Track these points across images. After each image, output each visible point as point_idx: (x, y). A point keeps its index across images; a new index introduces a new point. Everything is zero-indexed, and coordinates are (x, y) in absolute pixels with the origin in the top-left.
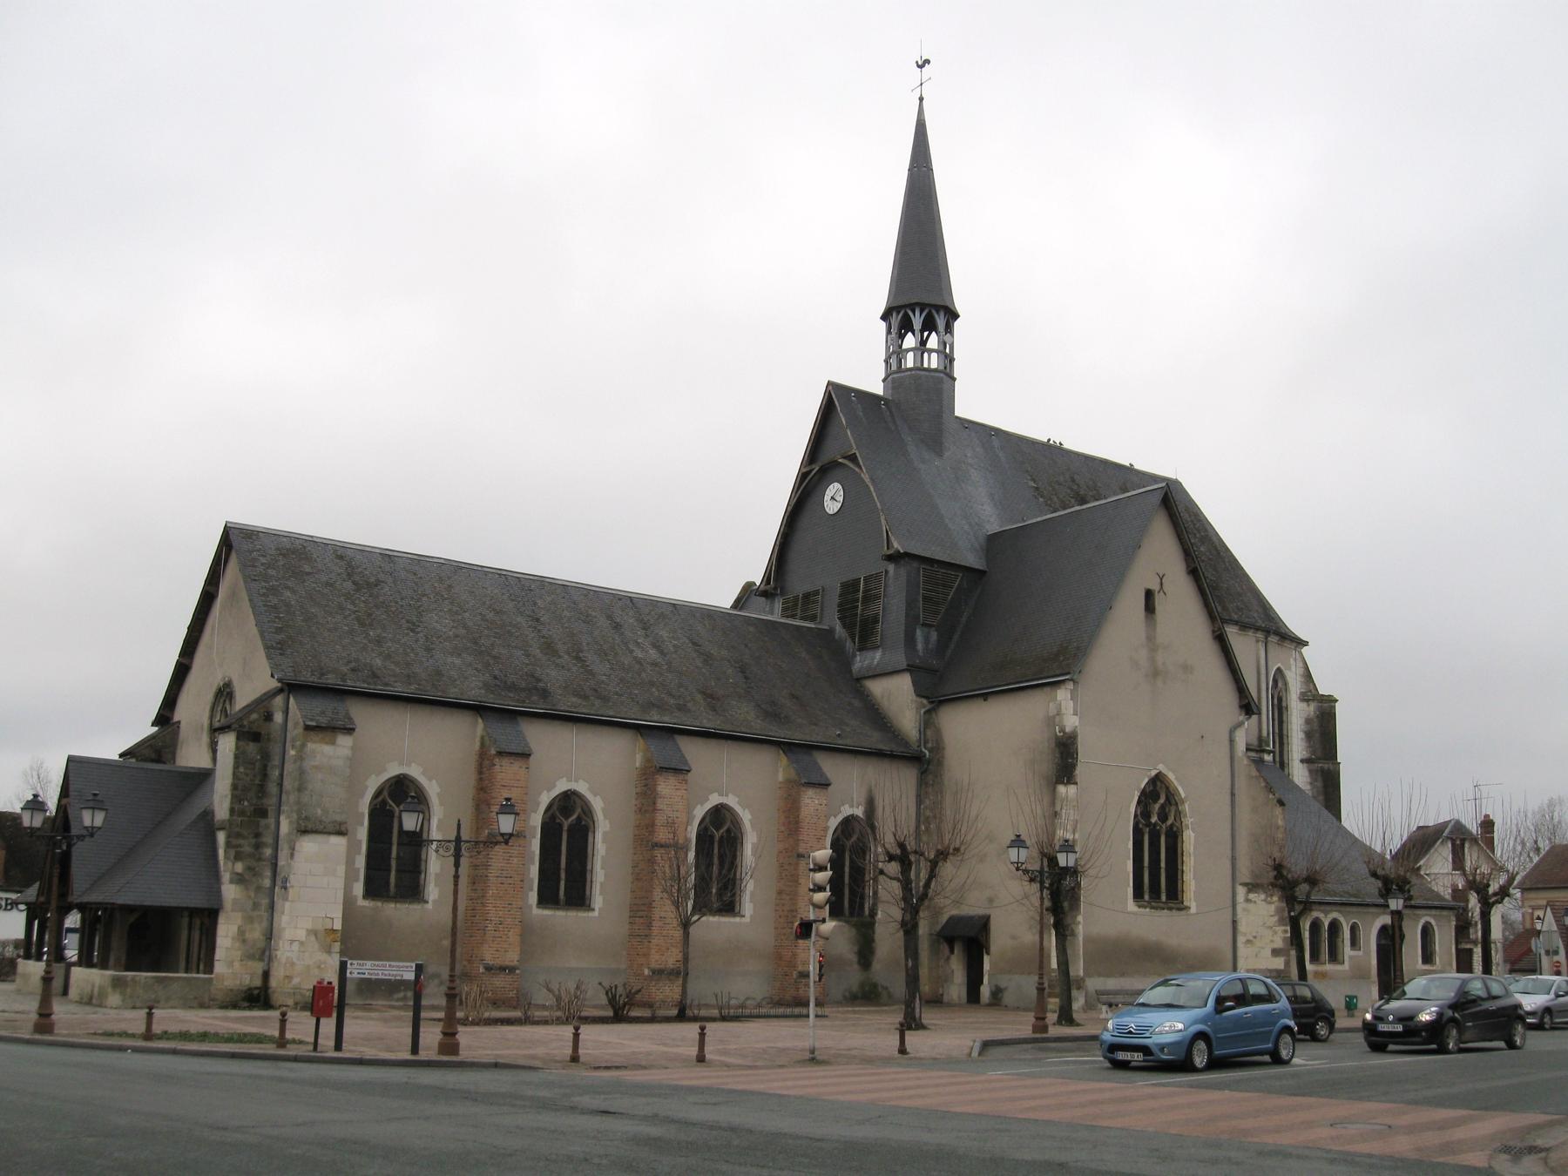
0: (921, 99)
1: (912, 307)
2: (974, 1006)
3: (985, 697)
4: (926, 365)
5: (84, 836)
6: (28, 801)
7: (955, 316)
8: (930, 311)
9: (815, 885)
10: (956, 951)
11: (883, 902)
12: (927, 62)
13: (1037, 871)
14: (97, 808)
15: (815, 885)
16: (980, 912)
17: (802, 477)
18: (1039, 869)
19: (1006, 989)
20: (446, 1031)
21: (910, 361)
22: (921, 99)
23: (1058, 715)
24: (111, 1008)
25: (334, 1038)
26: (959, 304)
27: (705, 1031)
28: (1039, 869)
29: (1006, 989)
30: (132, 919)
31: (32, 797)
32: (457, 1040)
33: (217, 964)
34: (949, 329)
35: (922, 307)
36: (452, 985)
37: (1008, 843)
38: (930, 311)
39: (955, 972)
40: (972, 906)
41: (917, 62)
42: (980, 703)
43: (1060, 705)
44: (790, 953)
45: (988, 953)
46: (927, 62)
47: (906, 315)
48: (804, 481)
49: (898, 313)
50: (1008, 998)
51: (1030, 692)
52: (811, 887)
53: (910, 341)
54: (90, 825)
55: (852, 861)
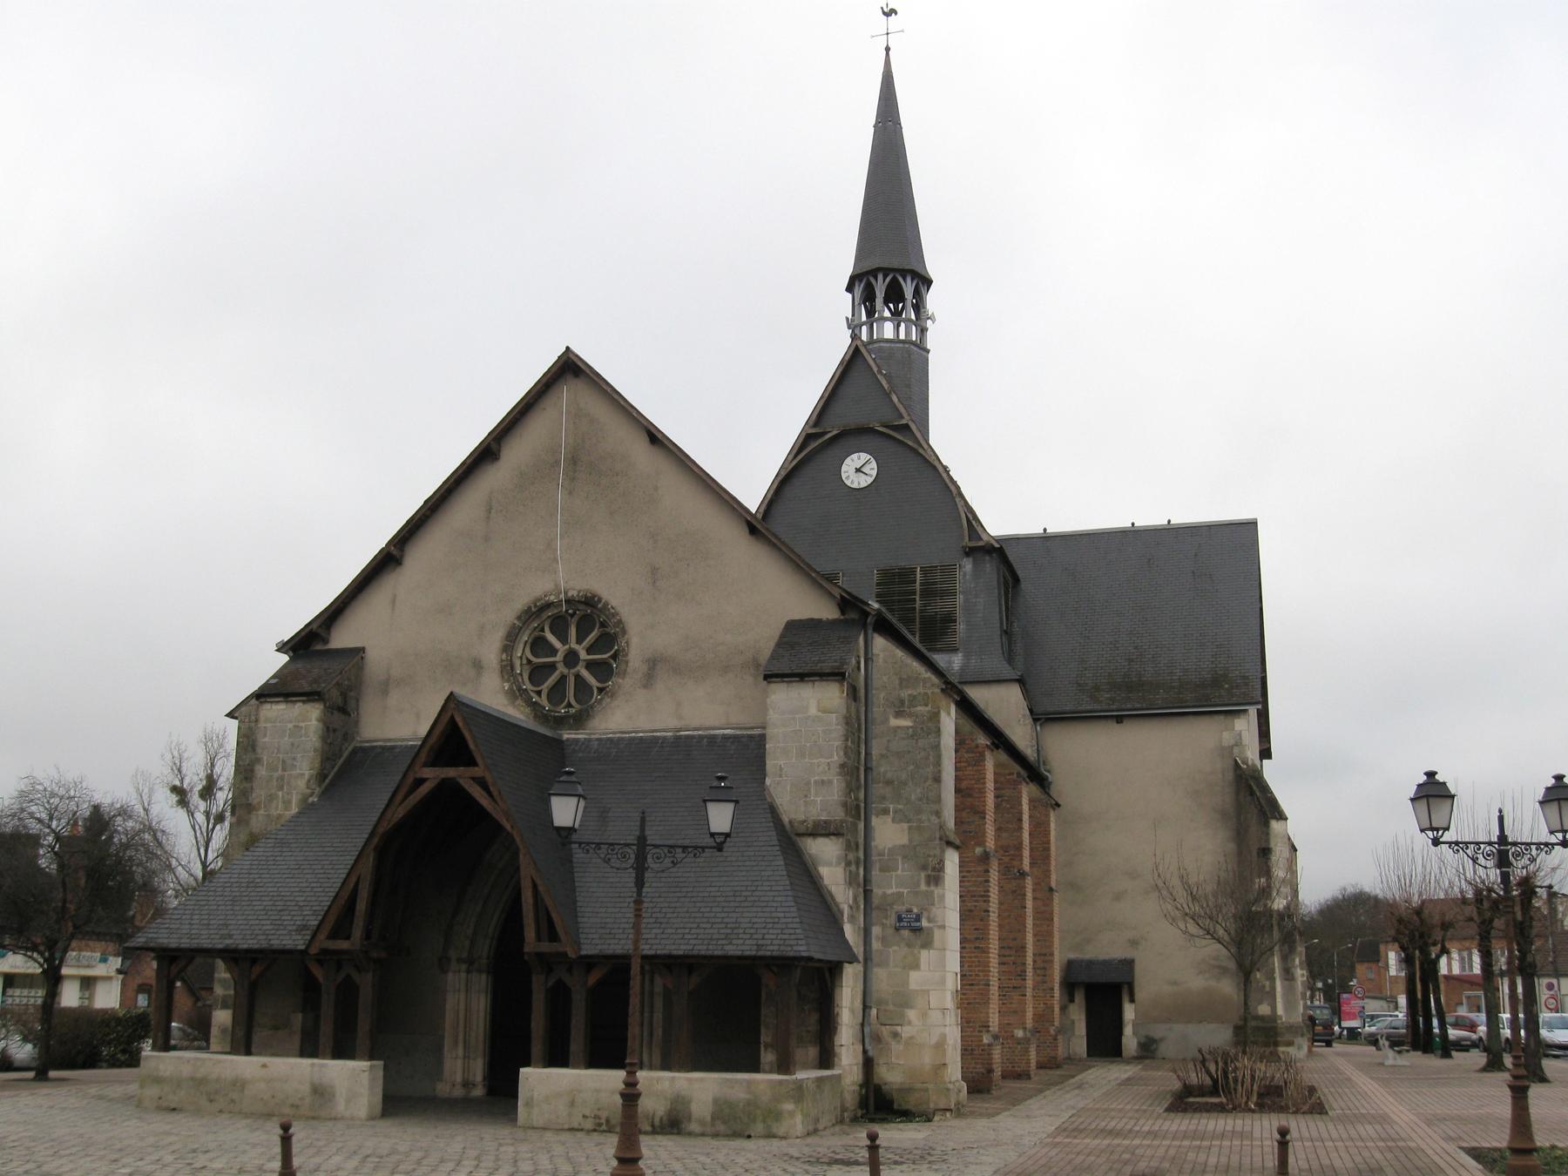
0: (888, 49)
1: (874, 273)
2: (1117, 1059)
3: (1119, 719)
5: (1553, 845)
6: (1548, 789)
8: (894, 280)
10: (1076, 1000)
11: (636, 942)
12: (893, 12)
14: (711, 801)
16: (1117, 953)
17: (806, 439)
19: (1162, 1040)
22: (888, 49)
23: (1237, 745)
24: (797, 1138)
25: (279, 1157)
29: (1162, 1040)
30: (592, 979)
31: (1553, 781)
33: (211, 1045)
35: (886, 271)
36: (631, 1080)
38: (868, 280)
39: (1077, 1024)
40: (1106, 948)
41: (882, 8)
42: (1113, 725)
43: (1240, 735)
44: (1042, 1005)
45: (1132, 1000)
46: (893, 12)
47: (895, 282)
50: (1164, 1049)
51: (1191, 718)
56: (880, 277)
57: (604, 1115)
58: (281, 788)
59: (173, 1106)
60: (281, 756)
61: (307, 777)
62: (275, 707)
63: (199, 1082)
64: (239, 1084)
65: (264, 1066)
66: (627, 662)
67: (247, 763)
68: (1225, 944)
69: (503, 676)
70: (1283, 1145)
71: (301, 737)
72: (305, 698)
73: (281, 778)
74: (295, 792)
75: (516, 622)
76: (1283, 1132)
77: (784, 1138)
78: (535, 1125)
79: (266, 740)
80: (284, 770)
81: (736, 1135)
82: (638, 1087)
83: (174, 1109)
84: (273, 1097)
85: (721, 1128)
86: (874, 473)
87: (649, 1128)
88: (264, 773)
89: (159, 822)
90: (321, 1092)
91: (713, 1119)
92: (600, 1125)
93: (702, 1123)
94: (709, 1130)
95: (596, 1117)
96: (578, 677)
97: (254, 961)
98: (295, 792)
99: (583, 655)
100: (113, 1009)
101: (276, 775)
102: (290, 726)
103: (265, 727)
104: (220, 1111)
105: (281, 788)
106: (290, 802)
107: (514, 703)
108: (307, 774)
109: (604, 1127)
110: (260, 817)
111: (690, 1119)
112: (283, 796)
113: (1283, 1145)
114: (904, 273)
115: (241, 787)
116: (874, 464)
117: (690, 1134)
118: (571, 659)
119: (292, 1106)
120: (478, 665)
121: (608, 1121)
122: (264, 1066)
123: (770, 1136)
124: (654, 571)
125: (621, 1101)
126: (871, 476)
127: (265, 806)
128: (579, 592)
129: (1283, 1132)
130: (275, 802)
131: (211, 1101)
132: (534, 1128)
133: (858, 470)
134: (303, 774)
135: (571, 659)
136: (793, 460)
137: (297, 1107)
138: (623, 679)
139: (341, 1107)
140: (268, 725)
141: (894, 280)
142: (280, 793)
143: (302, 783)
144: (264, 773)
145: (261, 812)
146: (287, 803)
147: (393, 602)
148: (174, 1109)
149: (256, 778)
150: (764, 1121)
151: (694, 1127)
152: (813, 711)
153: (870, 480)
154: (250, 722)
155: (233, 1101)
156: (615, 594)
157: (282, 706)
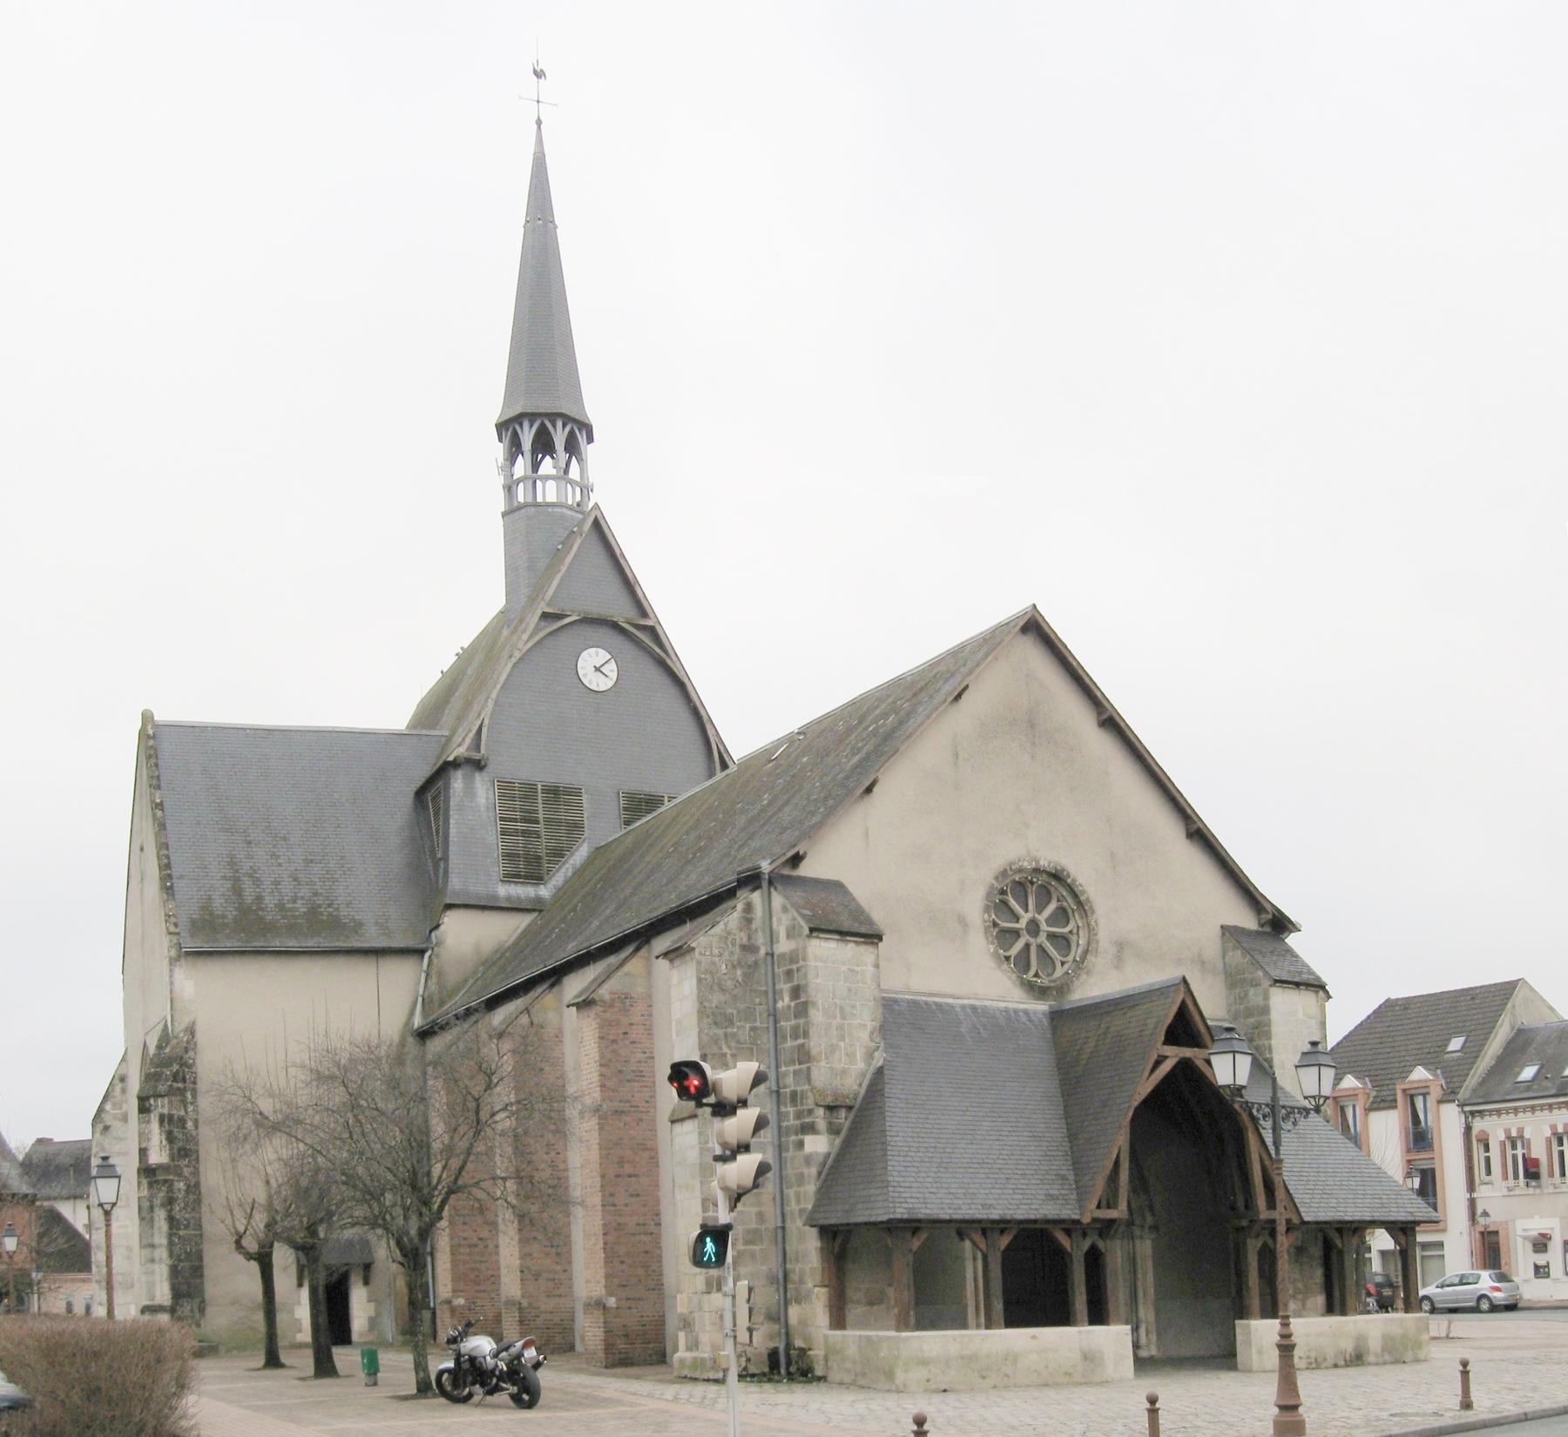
0: (539, 122)
4: (540, 499)
7: (588, 429)
8: (543, 425)
9: (724, 1145)
13: (1267, 1105)
15: (724, 1145)
18: (1268, 1100)
20: (1283, 1403)
21: (521, 495)
22: (539, 122)
26: (593, 411)
27: (1468, 1368)
28: (1268, 1100)
32: (1301, 1415)
34: (572, 447)
35: (532, 417)
36: (1285, 1332)
37: (1296, 1059)
48: (536, 634)
49: (507, 430)
52: (718, 1151)
53: (521, 467)
54: (1232, 1082)
55: (1521, 1092)
56: (559, 424)
57: (1313, 1355)
58: (842, 1038)
59: (943, 1387)
60: (838, 1002)
61: (869, 1028)
62: (824, 944)
63: (969, 1360)
64: (1011, 1358)
65: (1034, 1337)
66: (1098, 942)
67: (714, 1005)
68: (780, 1246)
69: (987, 938)
70: (1153, 1412)
71: (858, 982)
72: (862, 940)
73: (840, 1027)
74: (858, 1044)
75: (994, 882)
76: (1153, 1400)
77: (1425, 1361)
78: (1268, 1368)
79: (819, 981)
80: (843, 1017)
81: (1396, 1362)
82: (1293, 1338)
83: (945, 1391)
84: (1047, 1367)
85: (1387, 1357)
86: (614, 676)
87: (1343, 1363)
88: (820, 1019)
89: (338, 1064)
90: (1090, 1358)
91: (1383, 1351)
92: (1311, 1363)
93: (1376, 1355)
94: (1381, 1360)
95: (1308, 1357)
96: (1041, 948)
97: (915, 1231)
98: (858, 1044)
99: (1044, 927)
100: (675, 1306)
101: (834, 1023)
102: (844, 968)
103: (816, 967)
104: (995, 1387)
105: (842, 1038)
106: (854, 1055)
107: (1000, 966)
108: (870, 1025)
109: (1314, 1366)
110: (823, 1070)
111: (1368, 1353)
112: (845, 1048)
113: (1153, 1412)
114: (553, 417)
115: (711, 1033)
116: (613, 665)
117: (1369, 1364)
118: (1034, 928)
119: (1066, 1373)
120: (962, 921)
121: (1316, 1360)
122: (1034, 1337)
123: (1417, 1361)
124: (1113, 855)
125: (1278, 1352)
126: (611, 679)
127: (827, 1058)
128: (1050, 863)
129: (1153, 1400)
130: (837, 1054)
131: (984, 1378)
132: (1265, 1372)
133: (597, 669)
134: (865, 1025)
135: (1034, 928)
136: (528, 641)
137: (1070, 1374)
138: (1096, 957)
139: (1110, 1371)
140: (818, 964)
141: (543, 425)
142: (842, 1044)
143: (864, 1035)
144: (820, 1019)
145: (823, 1063)
146: (851, 1056)
147: (867, 835)
148: (945, 1391)
149: (813, 1024)
150: (1412, 1349)
151: (1371, 1358)
152: (1300, 1015)
153: (610, 684)
154: (711, 955)
155: (1006, 1375)
156: (1084, 874)
157: (832, 945)
